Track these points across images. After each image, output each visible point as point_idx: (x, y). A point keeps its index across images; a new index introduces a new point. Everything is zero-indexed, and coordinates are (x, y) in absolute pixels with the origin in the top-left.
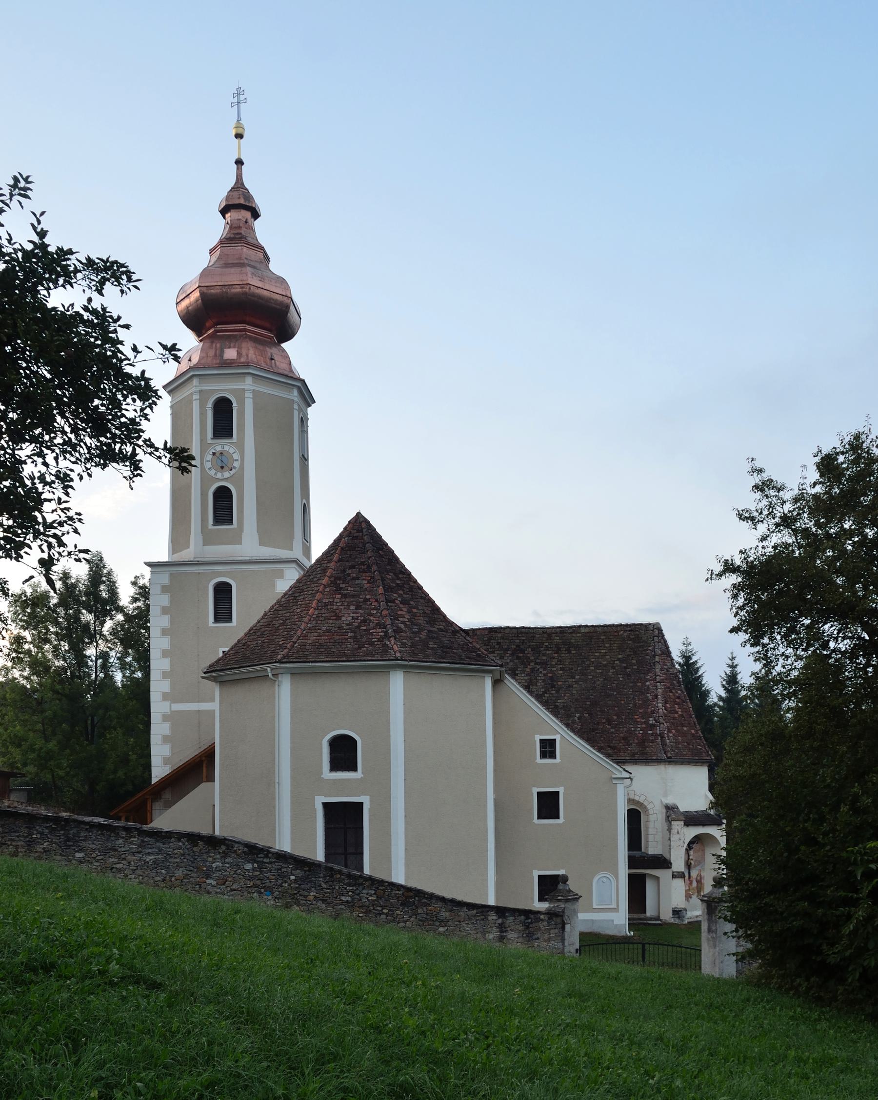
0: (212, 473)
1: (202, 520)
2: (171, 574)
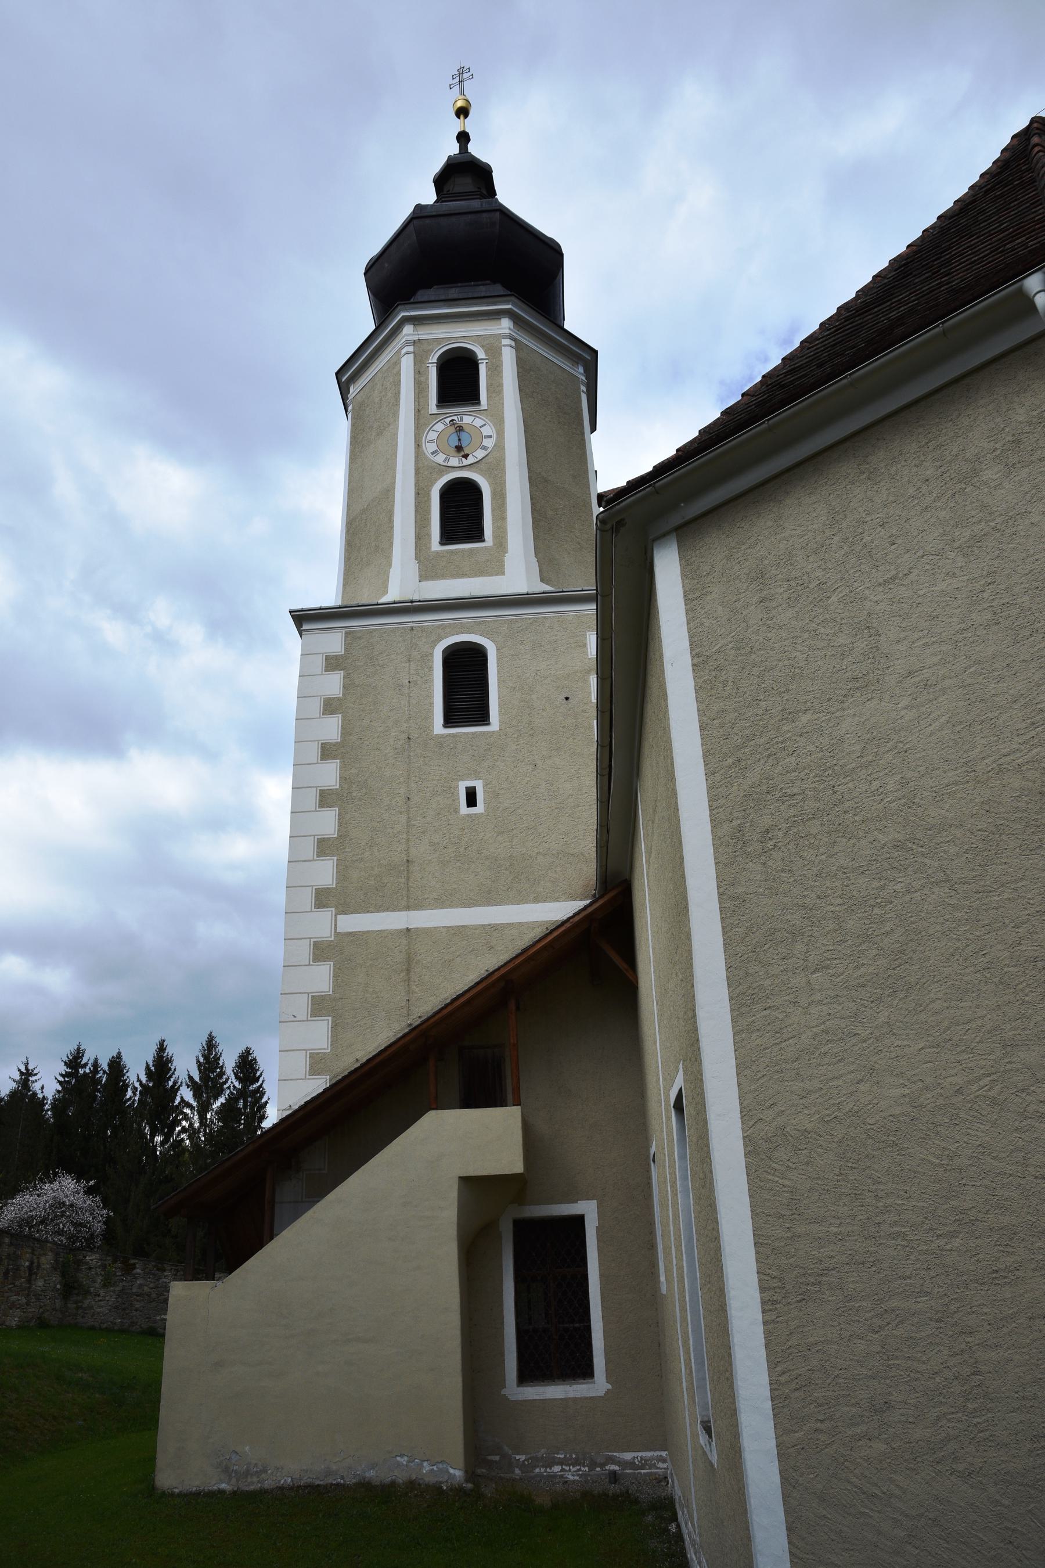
2: (346, 633)
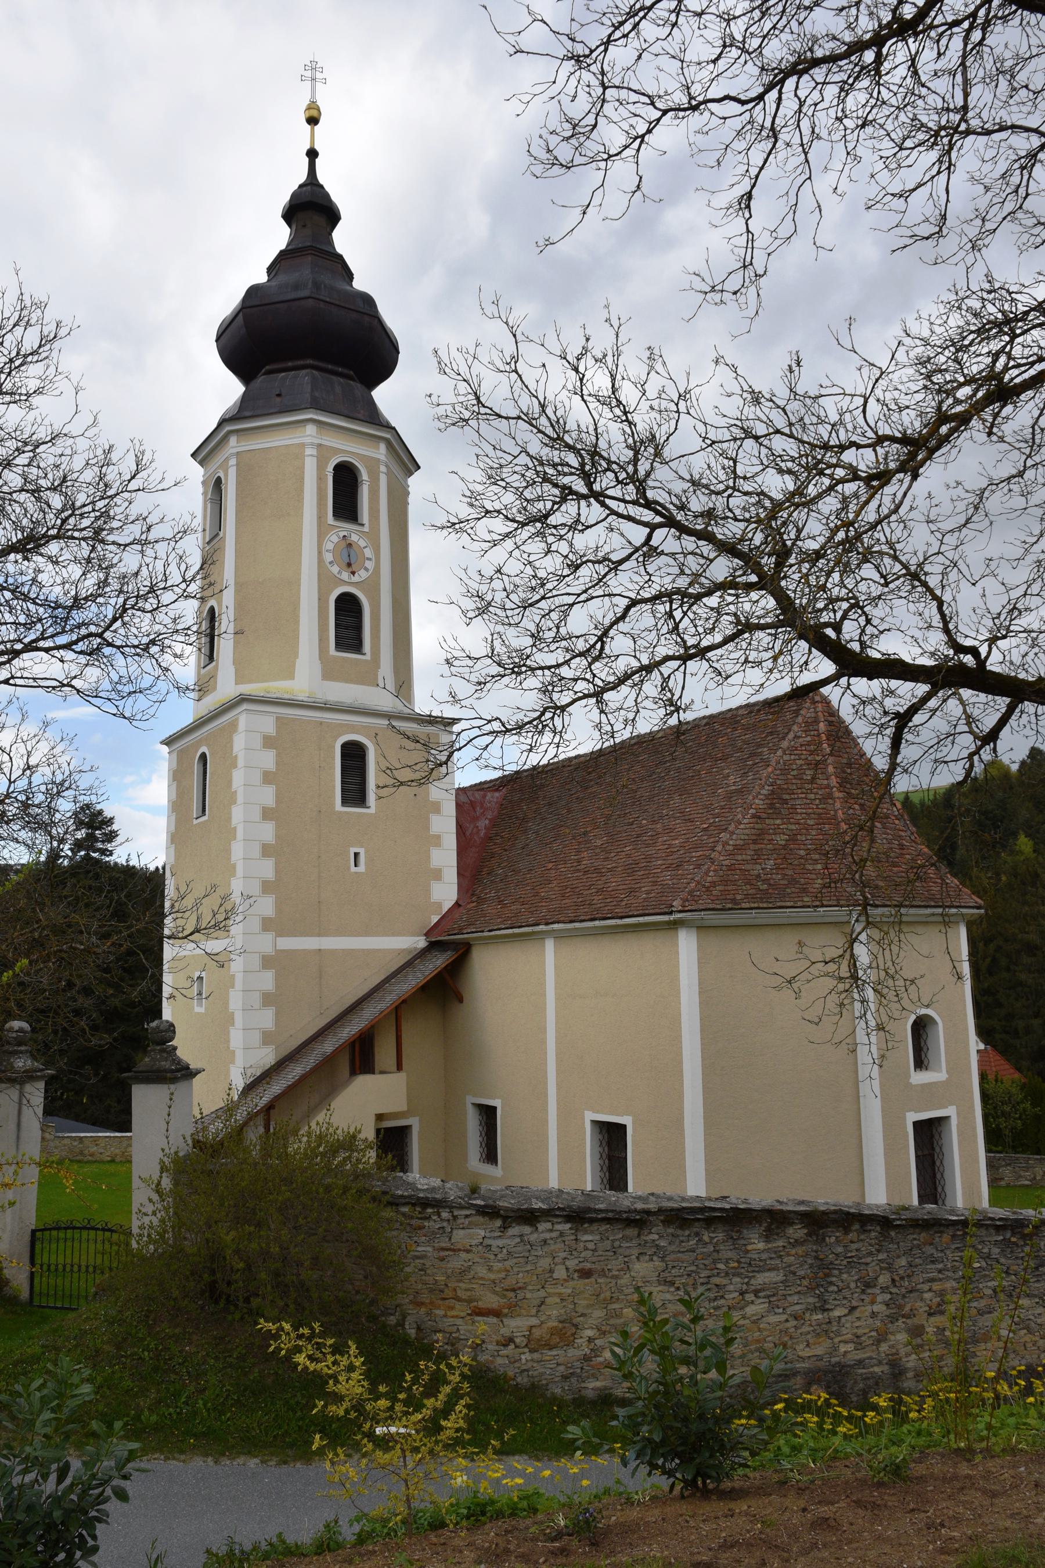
0: (335, 569)
1: (320, 640)
